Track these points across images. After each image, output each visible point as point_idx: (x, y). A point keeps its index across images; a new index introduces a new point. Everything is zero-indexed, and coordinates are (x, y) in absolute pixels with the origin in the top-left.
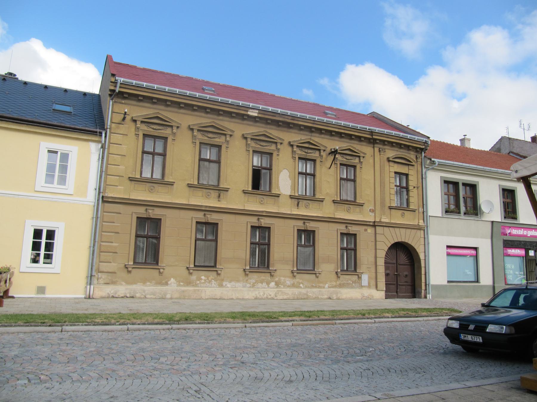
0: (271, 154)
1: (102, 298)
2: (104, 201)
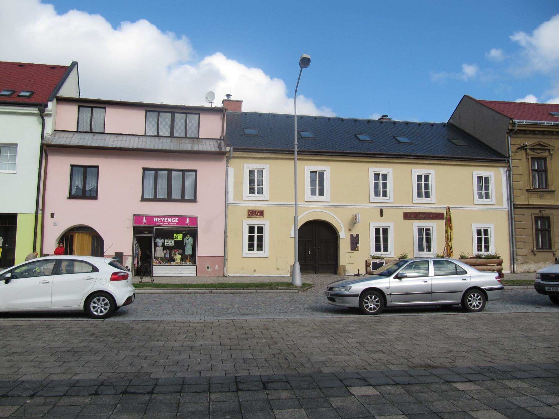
0: (545, 159)
1: (521, 273)
2: (514, 208)
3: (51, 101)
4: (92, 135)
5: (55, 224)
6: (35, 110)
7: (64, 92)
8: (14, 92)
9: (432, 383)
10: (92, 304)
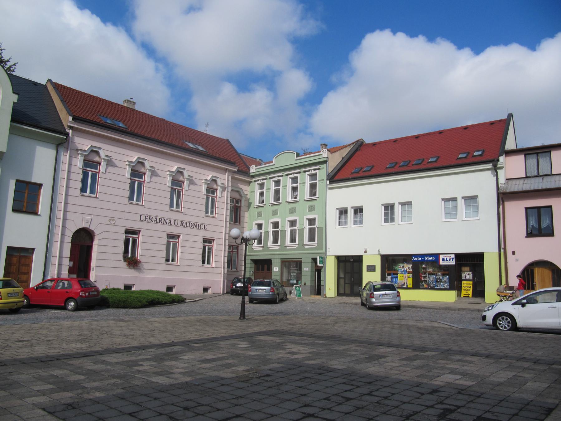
3: (502, 155)
4: (541, 178)
5: (517, 260)
6: (490, 166)
7: (510, 145)
8: (469, 153)
9: (301, 407)
10: (498, 321)
